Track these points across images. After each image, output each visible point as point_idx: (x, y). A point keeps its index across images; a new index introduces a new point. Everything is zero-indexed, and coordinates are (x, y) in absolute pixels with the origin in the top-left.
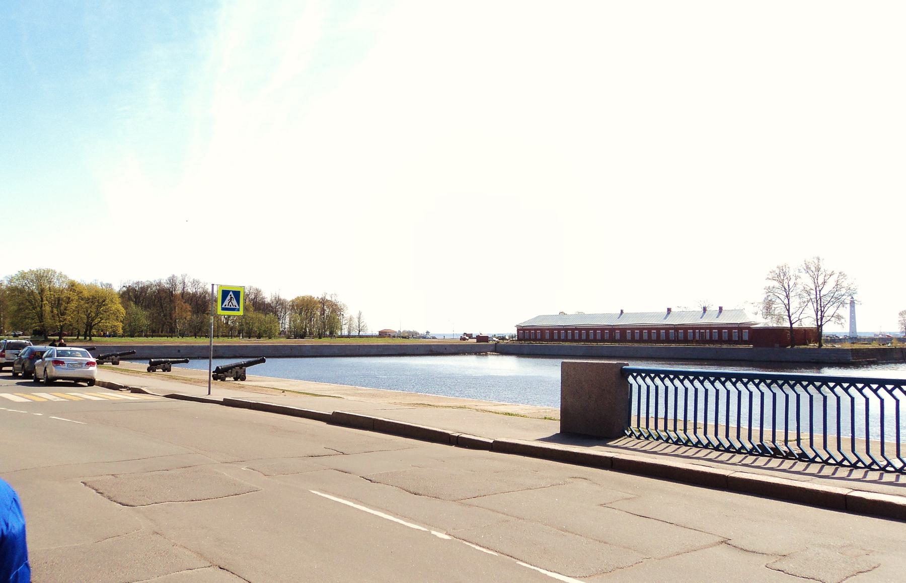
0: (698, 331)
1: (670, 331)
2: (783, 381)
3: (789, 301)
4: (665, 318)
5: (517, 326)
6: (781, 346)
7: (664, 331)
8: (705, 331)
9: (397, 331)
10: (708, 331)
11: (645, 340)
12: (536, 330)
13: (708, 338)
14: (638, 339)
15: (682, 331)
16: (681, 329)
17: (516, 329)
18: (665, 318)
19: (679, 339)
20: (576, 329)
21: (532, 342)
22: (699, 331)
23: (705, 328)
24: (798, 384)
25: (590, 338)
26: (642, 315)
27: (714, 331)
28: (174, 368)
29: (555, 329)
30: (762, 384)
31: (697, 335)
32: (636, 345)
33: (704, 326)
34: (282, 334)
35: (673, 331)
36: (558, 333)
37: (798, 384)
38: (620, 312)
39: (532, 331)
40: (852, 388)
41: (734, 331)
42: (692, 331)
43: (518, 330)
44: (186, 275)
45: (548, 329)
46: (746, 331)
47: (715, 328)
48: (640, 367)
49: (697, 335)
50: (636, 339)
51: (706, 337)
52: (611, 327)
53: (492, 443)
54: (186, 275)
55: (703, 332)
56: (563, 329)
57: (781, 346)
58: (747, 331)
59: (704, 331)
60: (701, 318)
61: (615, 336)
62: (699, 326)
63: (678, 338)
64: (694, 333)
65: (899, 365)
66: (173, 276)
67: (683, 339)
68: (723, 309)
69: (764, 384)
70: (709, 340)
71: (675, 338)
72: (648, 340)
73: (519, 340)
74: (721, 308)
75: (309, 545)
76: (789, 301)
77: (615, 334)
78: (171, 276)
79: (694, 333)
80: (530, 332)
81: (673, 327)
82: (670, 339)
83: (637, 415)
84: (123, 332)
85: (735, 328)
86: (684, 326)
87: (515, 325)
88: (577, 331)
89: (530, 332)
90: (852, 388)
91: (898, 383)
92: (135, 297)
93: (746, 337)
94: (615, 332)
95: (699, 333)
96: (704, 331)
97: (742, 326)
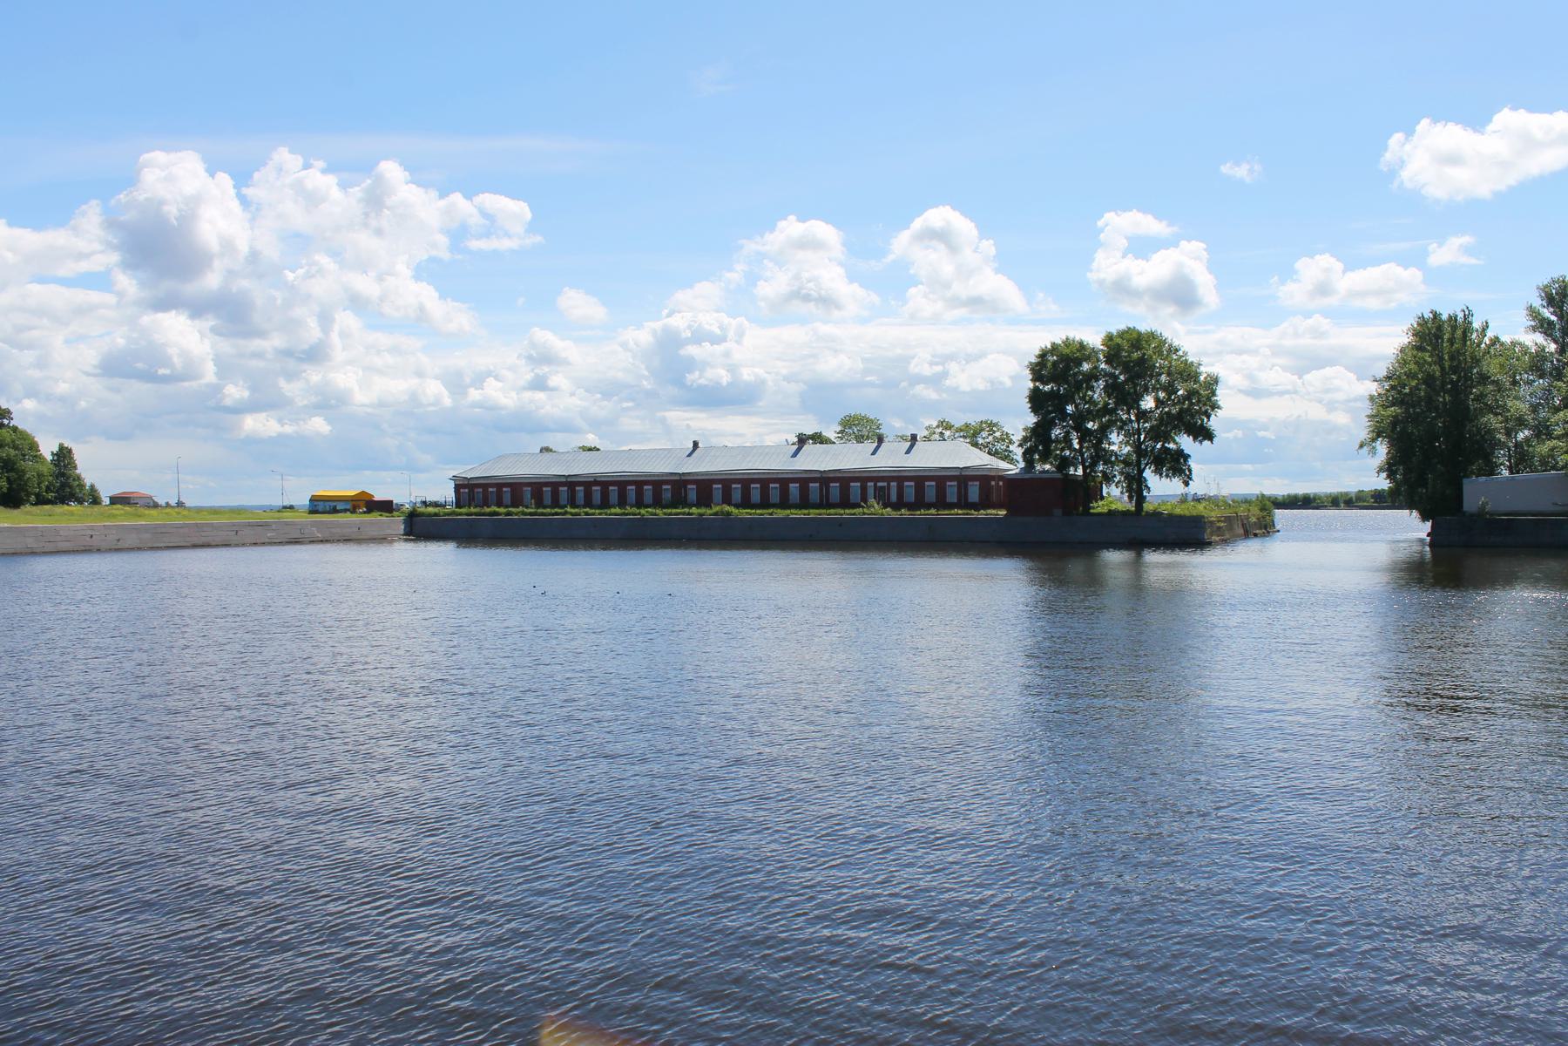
1: (811, 485)
4: (795, 455)
5: (455, 478)
12: (485, 486)
13: (894, 498)
14: (912, 499)
18: (795, 455)
20: (596, 483)
22: (875, 485)
29: (546, 484)
32: (813, 513)
35: (817, 485)
39: (490, 490)
41: (948, 483)
43: (457, 488)
59: (885, 484)
60: (598, 450)
61: (686, 495)
62: (875, 475)
63: (828, 499)
73: (458, 504)
77: (686, 491)
86: (840, 475)
92: (1452, 358)
93: (974, 493)
94: (828, 488)
96: (885, 484)
97: (967, 473)
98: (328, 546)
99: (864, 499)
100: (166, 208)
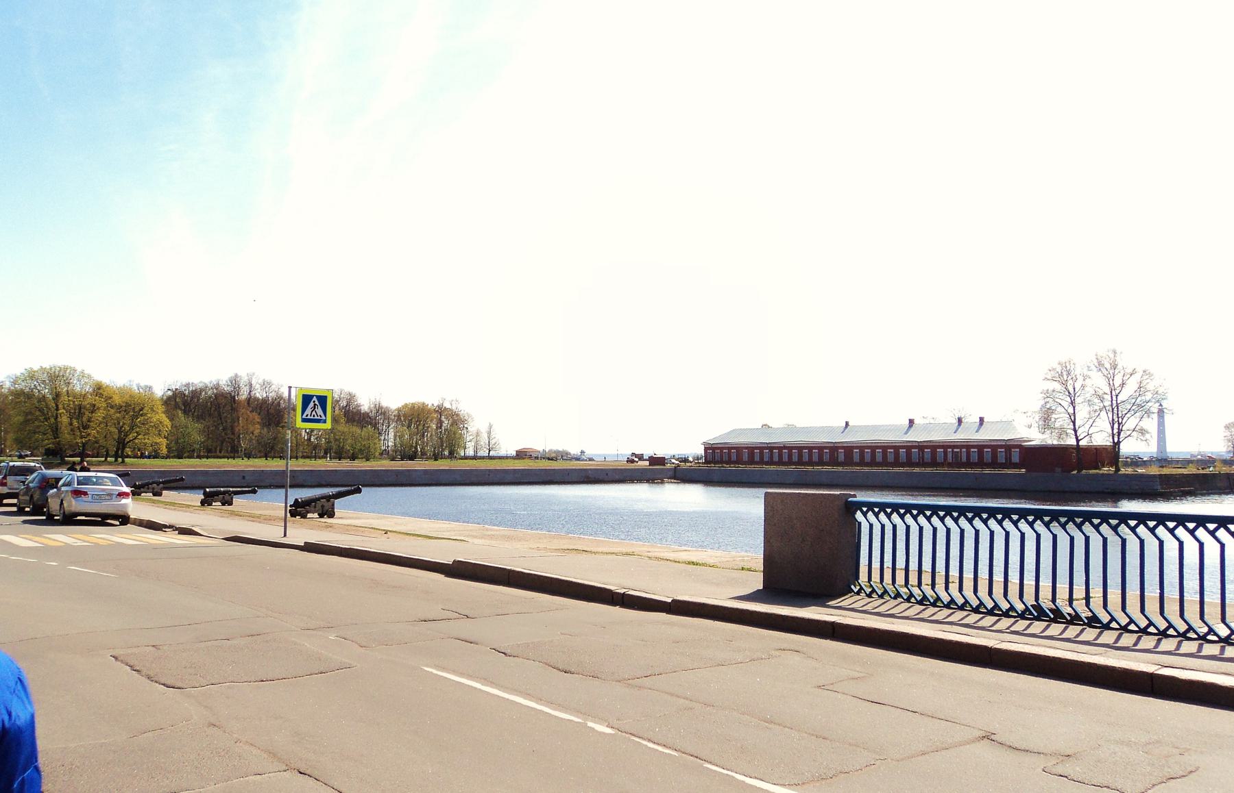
0: (950, 450)
1: (913, 450)
2: (1066, 519)
3: (1074, 410)
4: (906, 433)
5: (704, 443)
6: (1063, 471)
7: (905, 450)
8: (961, 450)
9: (541, 450)
10: (965, 450)
11: (879, 463)
12: (730, 449)
13: (964, 459)
14: (869, 461)
15: (929, 450)
16: (927, 447)
17: (702, 448)
18: (906, 433)
19: (925, 461)
20: (785, 447)
21: (725, 466)
22: (953, 451)
23: (961, 447)
24: (1087, 523)
25: (804, 460)
26: (875, 428)
27: (972, 450)
28: (237, 500)
29: (757, 448)
30: (1039, 522)
31: (950, 456)
32: (866, 469)
33: (958, 444)
34: (384, 454)
35: (917, 450)
36: (760, 453)
37: (1087, 523)
38: (844, 425)
39: (725, 451)
40: (1161, 528)
41: (999, 450)
42: (942, 450)
43: (706, 449)
44: (254, 374)
45: (746, 448)
46: (1016, 450)
47: (974, 447)
48: (872, 500)
49: (950, 456)
50: (866, 461)
51: (961, 459)
52: (832, 445)
53: (670, 603)
54: (254, 374)
55: (958, 452)
56: (766, 448)
57: (1063, 471)
58: (1018, 450)
59: (958, 450)
60: (955, 432)
61: (837, 457)
62: (952, 444)
63: (923, 460)
64: (945, 453)
65: (1224, 497)
66: (236, 375)
67: (930, 461)
68: (985, 420)
69: (1040, 523)
70: (965, 463)
71: (919, 460)
72: (883, 462)
73: (707, 462)
74: (982, 420)
75: (421, 742)
76: (1074, 410)
77: (837, 454)
78: (234, 375)
79: (945, 453)
80: (722, 452)
81: (917, 444)
82: (913, 461)
83: (867, 564)
84: (168, 452)
85: (1001, 447)
86: (931, 444)
87: (702, 442)
88: (786, 451)
89: (722, 452)
90: (1161, 528)
91: (1223, 522)
93: (1016, 458)
94: (838, 451)
95: (952, 454)
96: (958, 450)
97: (1011, 443)
98: (922, 623)
99: (216, 452)
100: (362, 408)
